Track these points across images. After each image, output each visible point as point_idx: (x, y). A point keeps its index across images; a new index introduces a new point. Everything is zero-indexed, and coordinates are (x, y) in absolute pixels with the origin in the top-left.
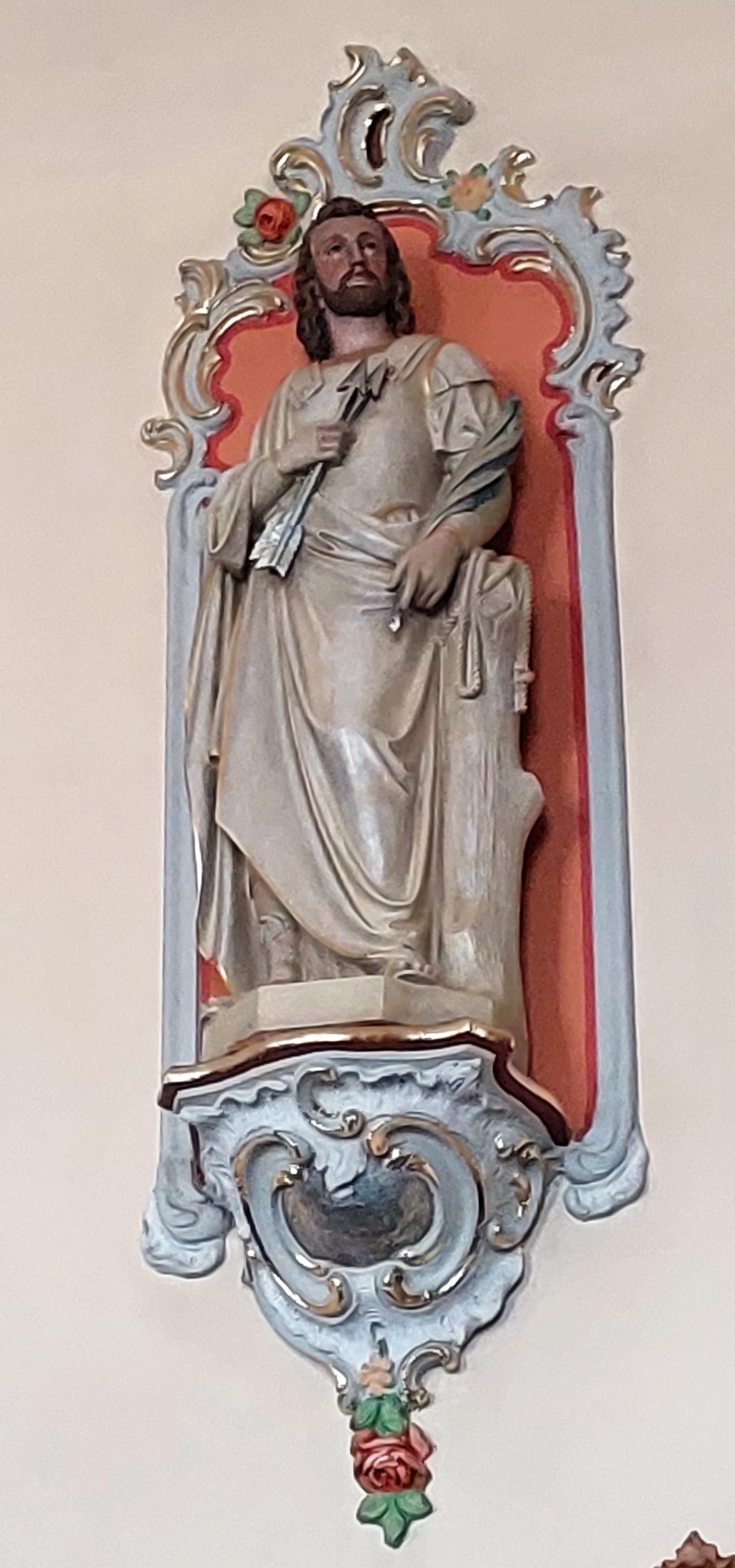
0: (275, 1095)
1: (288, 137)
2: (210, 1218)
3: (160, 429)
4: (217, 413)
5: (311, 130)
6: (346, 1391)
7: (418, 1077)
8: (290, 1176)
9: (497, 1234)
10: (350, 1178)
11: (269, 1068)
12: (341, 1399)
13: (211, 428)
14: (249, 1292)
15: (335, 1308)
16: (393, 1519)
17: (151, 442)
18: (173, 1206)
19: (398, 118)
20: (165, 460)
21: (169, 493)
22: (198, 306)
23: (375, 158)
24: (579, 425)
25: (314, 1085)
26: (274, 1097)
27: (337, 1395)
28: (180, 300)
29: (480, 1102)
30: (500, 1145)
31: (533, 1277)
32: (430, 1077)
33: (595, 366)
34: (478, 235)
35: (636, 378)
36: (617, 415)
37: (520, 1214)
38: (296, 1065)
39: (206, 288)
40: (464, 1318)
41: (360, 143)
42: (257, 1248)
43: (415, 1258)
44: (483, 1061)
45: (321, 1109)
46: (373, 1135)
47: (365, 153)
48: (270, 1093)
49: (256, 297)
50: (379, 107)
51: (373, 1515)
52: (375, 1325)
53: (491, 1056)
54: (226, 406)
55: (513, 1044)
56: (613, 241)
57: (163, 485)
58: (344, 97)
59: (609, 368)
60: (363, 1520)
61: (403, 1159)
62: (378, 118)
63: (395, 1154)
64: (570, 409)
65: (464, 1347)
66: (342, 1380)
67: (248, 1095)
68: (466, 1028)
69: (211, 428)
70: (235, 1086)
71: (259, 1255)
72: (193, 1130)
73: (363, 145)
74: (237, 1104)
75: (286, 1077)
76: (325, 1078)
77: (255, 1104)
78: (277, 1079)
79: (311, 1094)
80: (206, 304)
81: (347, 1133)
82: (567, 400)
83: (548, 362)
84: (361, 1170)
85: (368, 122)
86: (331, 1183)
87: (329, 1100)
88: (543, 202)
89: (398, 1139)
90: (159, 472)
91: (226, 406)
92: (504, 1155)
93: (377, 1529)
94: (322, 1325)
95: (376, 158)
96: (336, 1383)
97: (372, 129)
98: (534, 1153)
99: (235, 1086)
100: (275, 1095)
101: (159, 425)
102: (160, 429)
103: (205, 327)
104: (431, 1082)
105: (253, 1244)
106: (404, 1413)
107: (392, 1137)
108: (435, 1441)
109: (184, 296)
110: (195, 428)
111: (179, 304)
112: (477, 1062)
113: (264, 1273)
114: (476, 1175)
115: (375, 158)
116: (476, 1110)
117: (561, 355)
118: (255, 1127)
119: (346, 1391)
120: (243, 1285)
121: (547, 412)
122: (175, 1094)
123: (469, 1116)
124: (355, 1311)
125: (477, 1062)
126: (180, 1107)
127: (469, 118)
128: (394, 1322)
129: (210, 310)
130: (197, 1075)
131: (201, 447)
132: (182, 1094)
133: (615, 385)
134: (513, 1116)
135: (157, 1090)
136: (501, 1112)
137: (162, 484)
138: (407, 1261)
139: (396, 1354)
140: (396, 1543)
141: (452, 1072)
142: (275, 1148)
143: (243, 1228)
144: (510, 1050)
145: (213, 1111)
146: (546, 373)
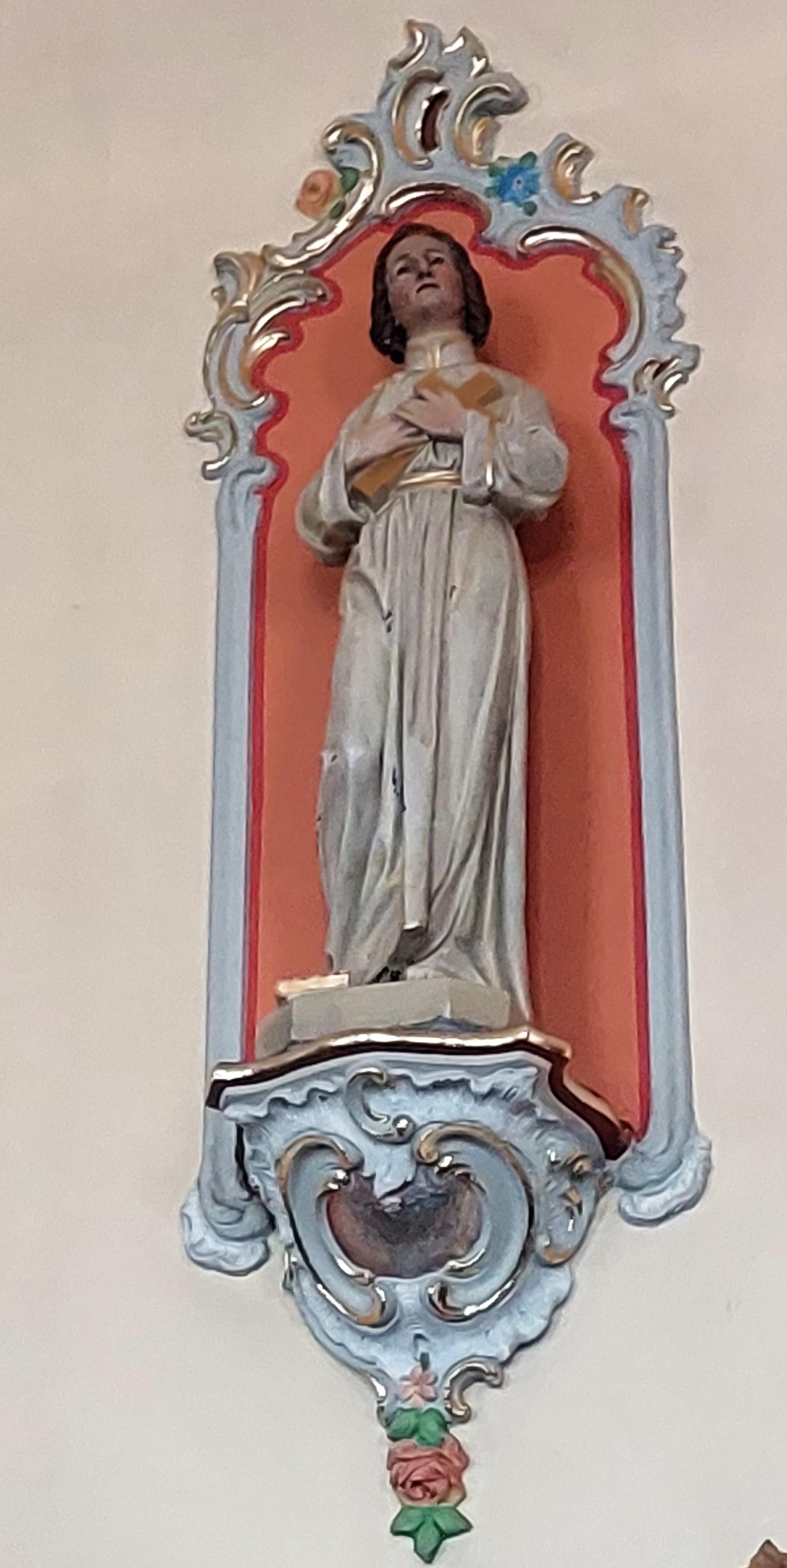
0: (325, 1097)
1: (346, 111)
2: (253, 1219)
3: (205, 421)
4: (263, 402)
5: (367, 105)
6: (384, 1404)
7: (473, 1085)
8: (336, 1181)
9: (547, 1247)
10: (398, 1183)
11: (325, 1066)
12: (381, 1410)
13: (258, 418)
14: (288, 1299)
15: (377, 1318)
16: (429, 1536)
17: (192, 434)
18: (217, 1202)
19: (453, 101)
20: (210, 450)
21: (218, 482)
22: (237, 298)
23: (428, 141)
24: (633, 423)
25: (365, 1086)
26: (323, 1099)
27: (376, 1406)
28: (216, 294)
29: (534, 1112)
30: (553, 1159)
31: (577, 1297)
32: (482, 1085)
33: (651, 363)
34: (524, 230)
35: (691, 376)
36: (671, 414)
37: (570, 1228)
38: (346, 1066)
39: (244, 278)
40: (509, 1331)
41: (415, 122)
42: (299, 1254)
43: (461, 1270)
44: (540, 1070)
45: (431, 1088)
46: (424, 1143)
47: (419, 135)
48: (320, 1094)
49: (296, 287)
50: (437, 90)
51: (407, 1528)
52: (419, 1336)
53: (547, 1065)
54: (271, 396)
55: (568, 1054)
56: (666, 237)
57: (209, 476)
58: (401, 77)
59: (663, 366)
60: (396, 1533)
61: (452, 1167)
62: (437, 101)
63: (446, 1162)
64: (624, 406)
65: (506, 1363)
66: (382, 1391)
67: (297, 1097)
68: (522, 1035)
69: (261, 417)
70: (283, 1086)
71: (302, 1262)
72: (240, 1131)
73: (419, 125)
74: (284, 1103)
75: (336, 1079)
76: (377, 1080)
77: (303, 1106)
78: (326, 1079)
79: (363, 1100)
80: (245, 297)
81: (396, 1137)
82: (624, 395)
83: (605, 360)
84: (409, 1179)
85: (426, 104)
86: (379, 1190)
87: (377, 1103)
88: (589, 199)
89: (451, 1146)
90: (206, 463)
91: (271, 396)
92: (556, 1167)
93: (409, 1542)
94: (364, 1335)
95: (428, 140)
96: (377, 1394)
97: (428, 111)
98: (584, 1165)
99: (283, 1086)
100: (325, 1097)
101: (202, 417)
102: (205, 421)
103: (247, 320)
104: (485, 1089)
105: (296, 1250)
106: (445, 1426)
107: (443, 1144)
108: (472, 1455)
109: (221, 289)
110: (240, 420)
111: (216, 298)
112: (533, 1070)
113: (306, 1281)
114: (526, 1184)
115: (428, 141)
116: (527, 1122)
117: (616, 353)
118: (303, 1128)
119: (384, 1404)
120: (285, 1291)
121: (600, 413)
122: (222, 1089)
123: (520, 1129)
124: (398, 1322)
125: (533, 1070)
126: (226, 1106)
127: (522, 106)
128: (437, 1333)
129: (247, 302)
130: (248, 1072)
131: (246, 437)
132: (229, 1091)
133: (668, 385)
134: (568, 1127)
135: (201, 1094)
136: (554, 1122)
137: (208, 474)
138: (454, 1272)
139: (438, 1365)
140: (429, 1558)
141: (507, 1080)
142: (326, 1151)
143: (285, 1232)
144: (566, 1060)
145: (261, 1111)
146: (600, 372)
